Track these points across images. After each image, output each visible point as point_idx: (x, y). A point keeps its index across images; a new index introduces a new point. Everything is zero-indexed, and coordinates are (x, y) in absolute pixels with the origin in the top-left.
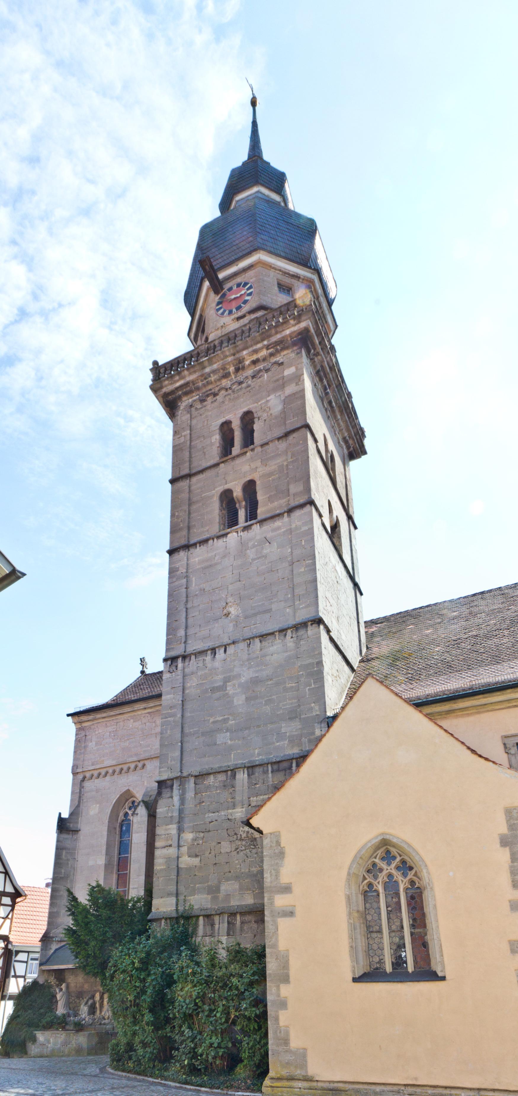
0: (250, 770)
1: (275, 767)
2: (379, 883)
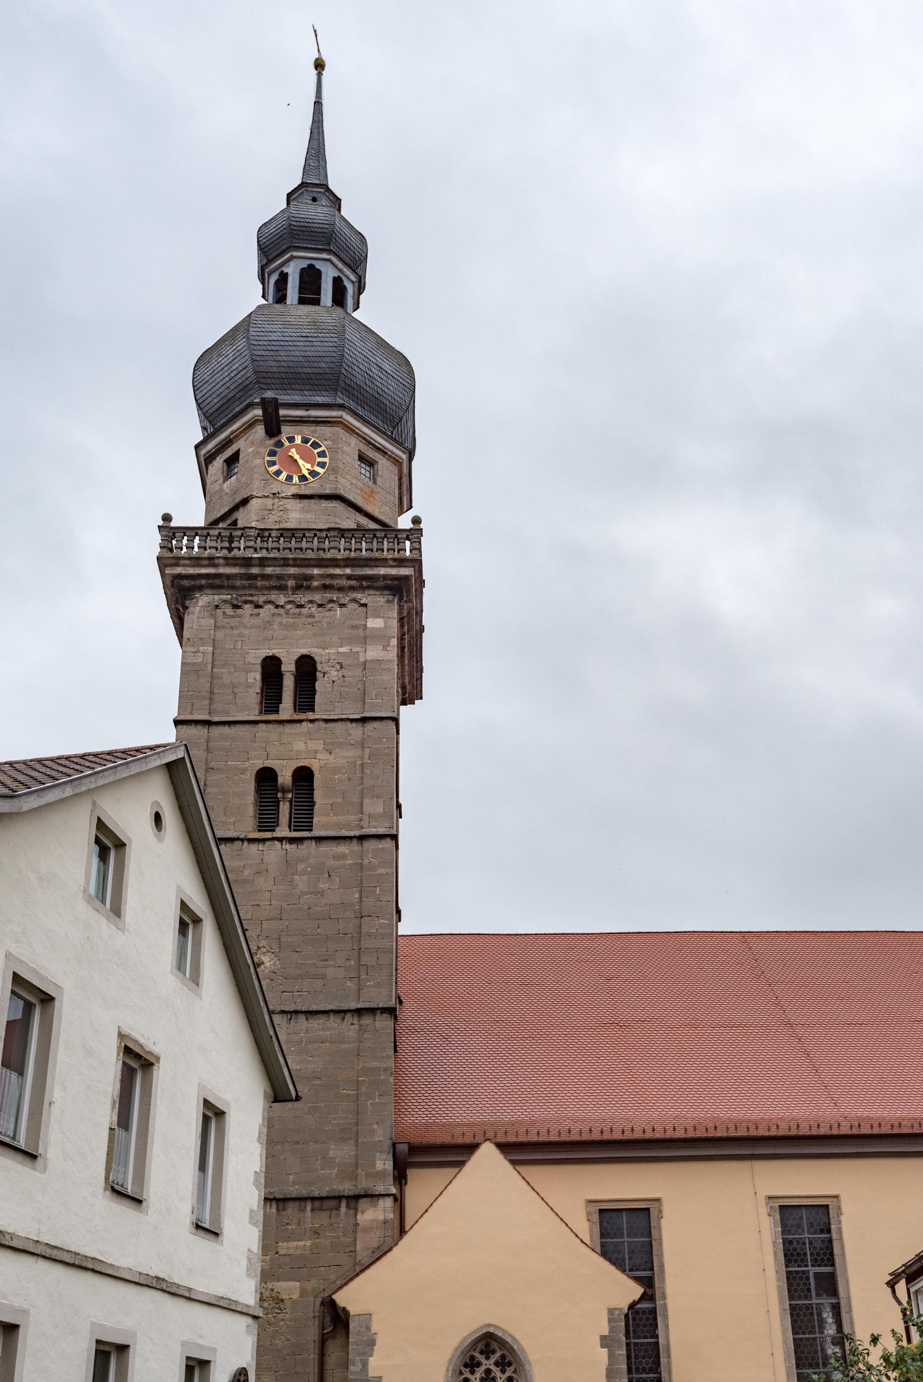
0: (281, 1204)
1: (317, 1204)
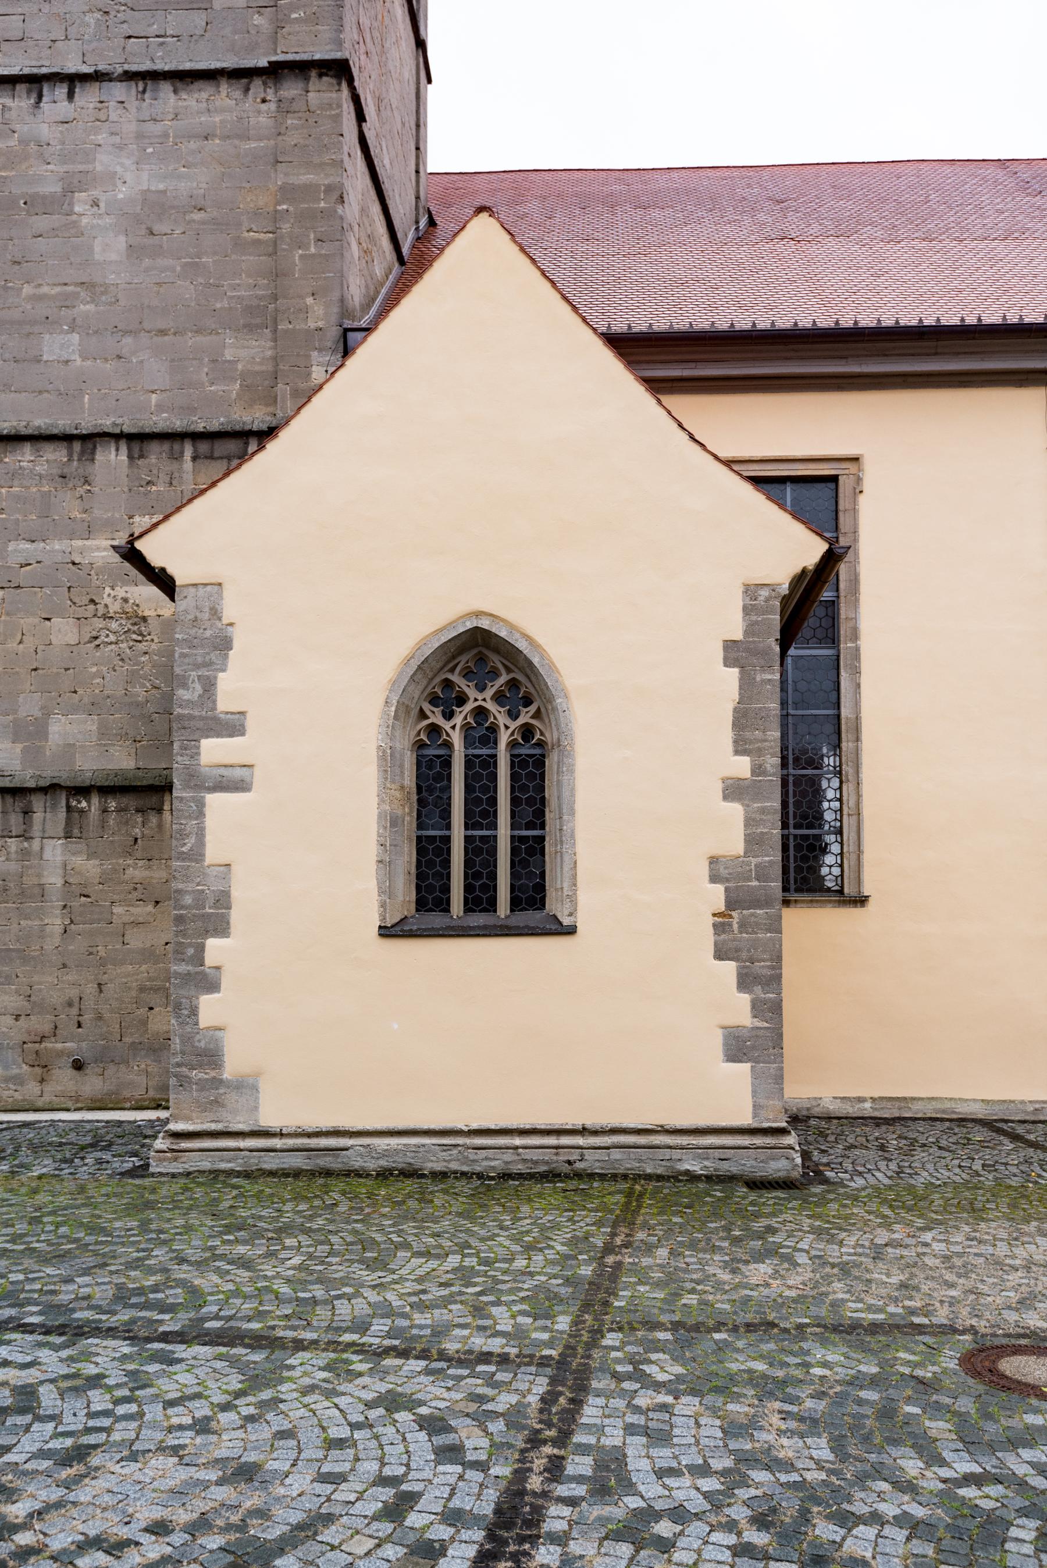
0: (136, 447)
1: (204, 447)
2: (453, 727)
